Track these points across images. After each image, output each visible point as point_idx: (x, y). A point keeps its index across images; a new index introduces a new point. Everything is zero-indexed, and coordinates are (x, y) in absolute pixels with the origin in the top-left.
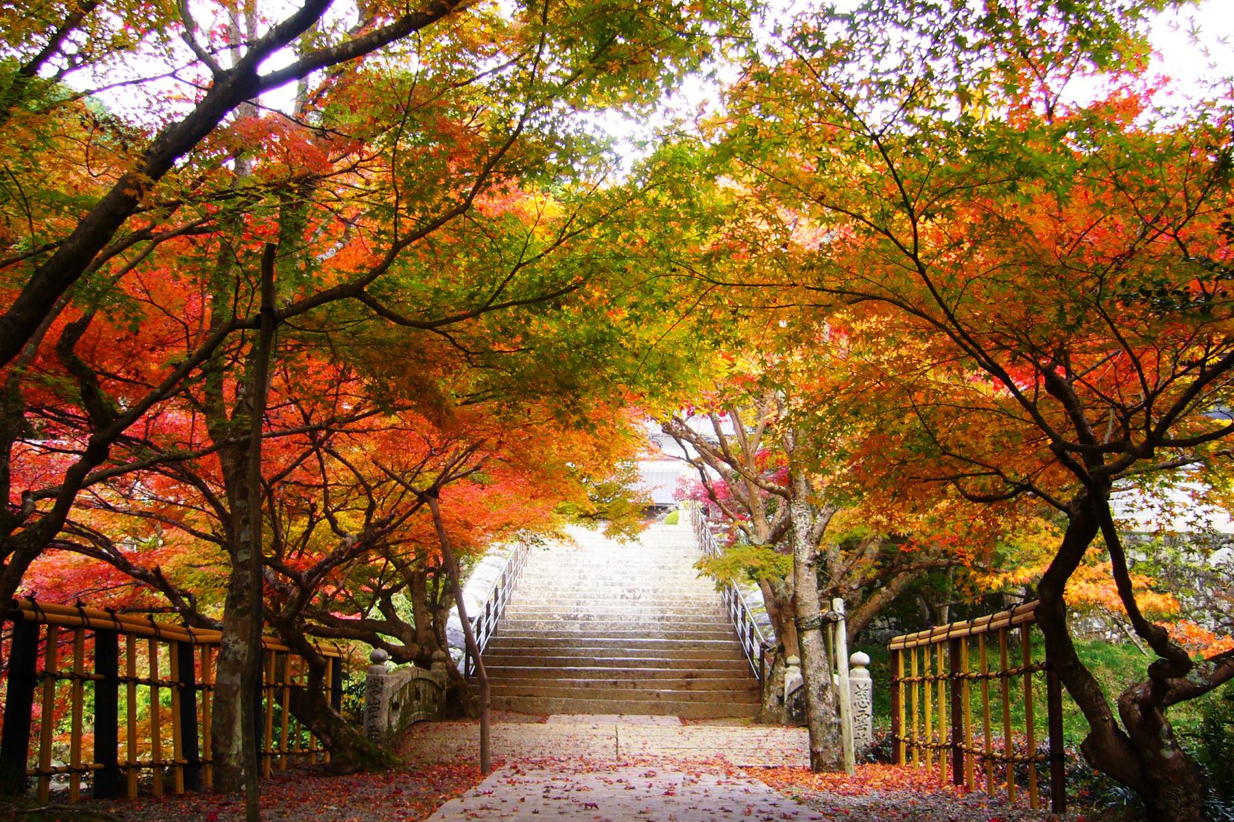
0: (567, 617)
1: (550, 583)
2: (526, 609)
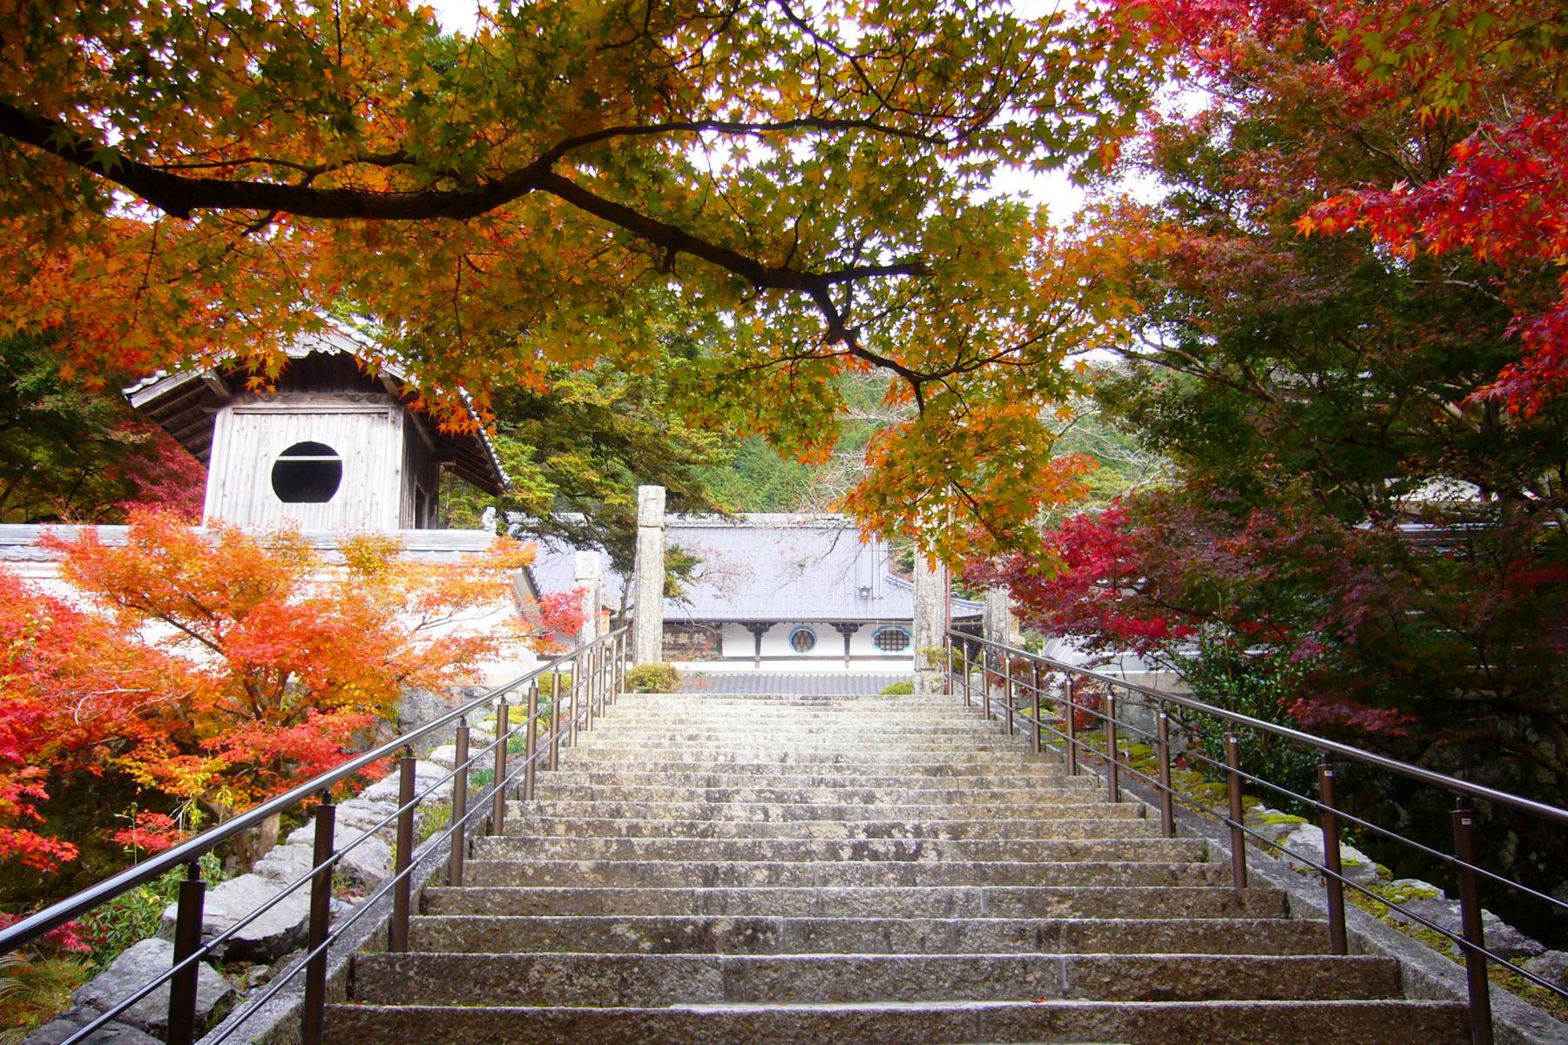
0: (670, 938)
1: (617, 813)
2: (512, 902)
